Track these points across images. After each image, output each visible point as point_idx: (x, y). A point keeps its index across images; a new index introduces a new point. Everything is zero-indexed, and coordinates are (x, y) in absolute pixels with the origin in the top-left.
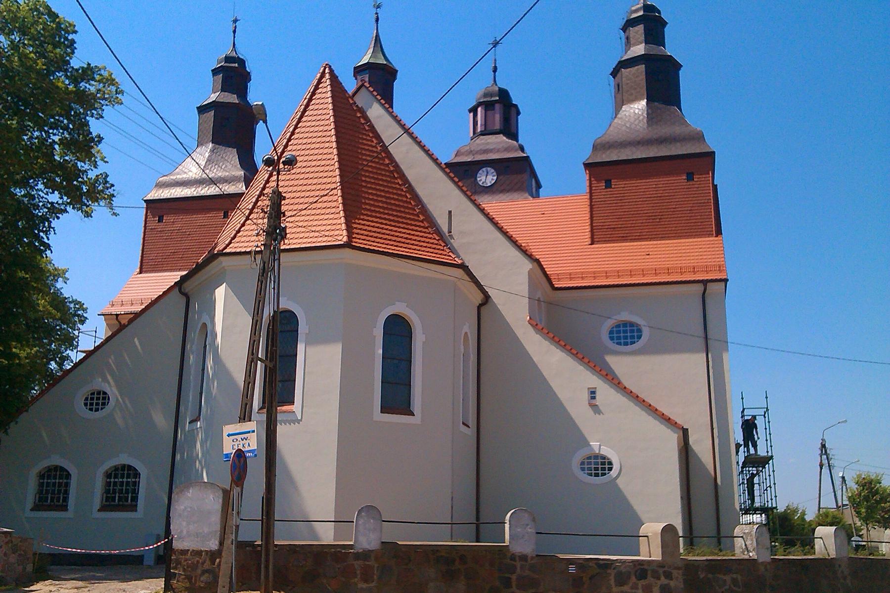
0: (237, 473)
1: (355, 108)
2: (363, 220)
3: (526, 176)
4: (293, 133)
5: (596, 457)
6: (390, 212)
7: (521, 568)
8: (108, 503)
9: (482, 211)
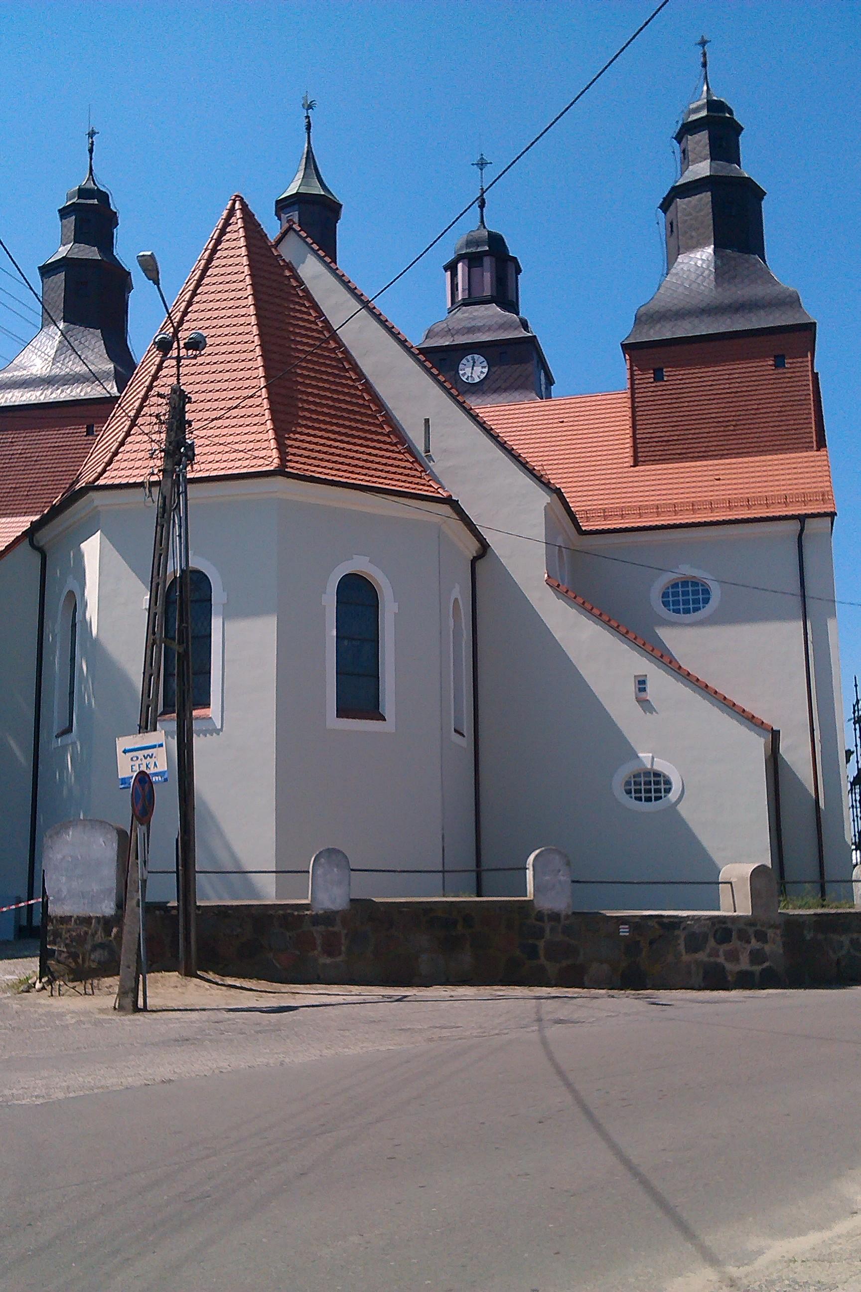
0: (140, 807)
1: (282, 263)
2: (301, 433)
3: (531, 367)
4: (190, 303)
5: (647, 773)
6: (341, 422)
7: (552, 929)
9: (475, 418)
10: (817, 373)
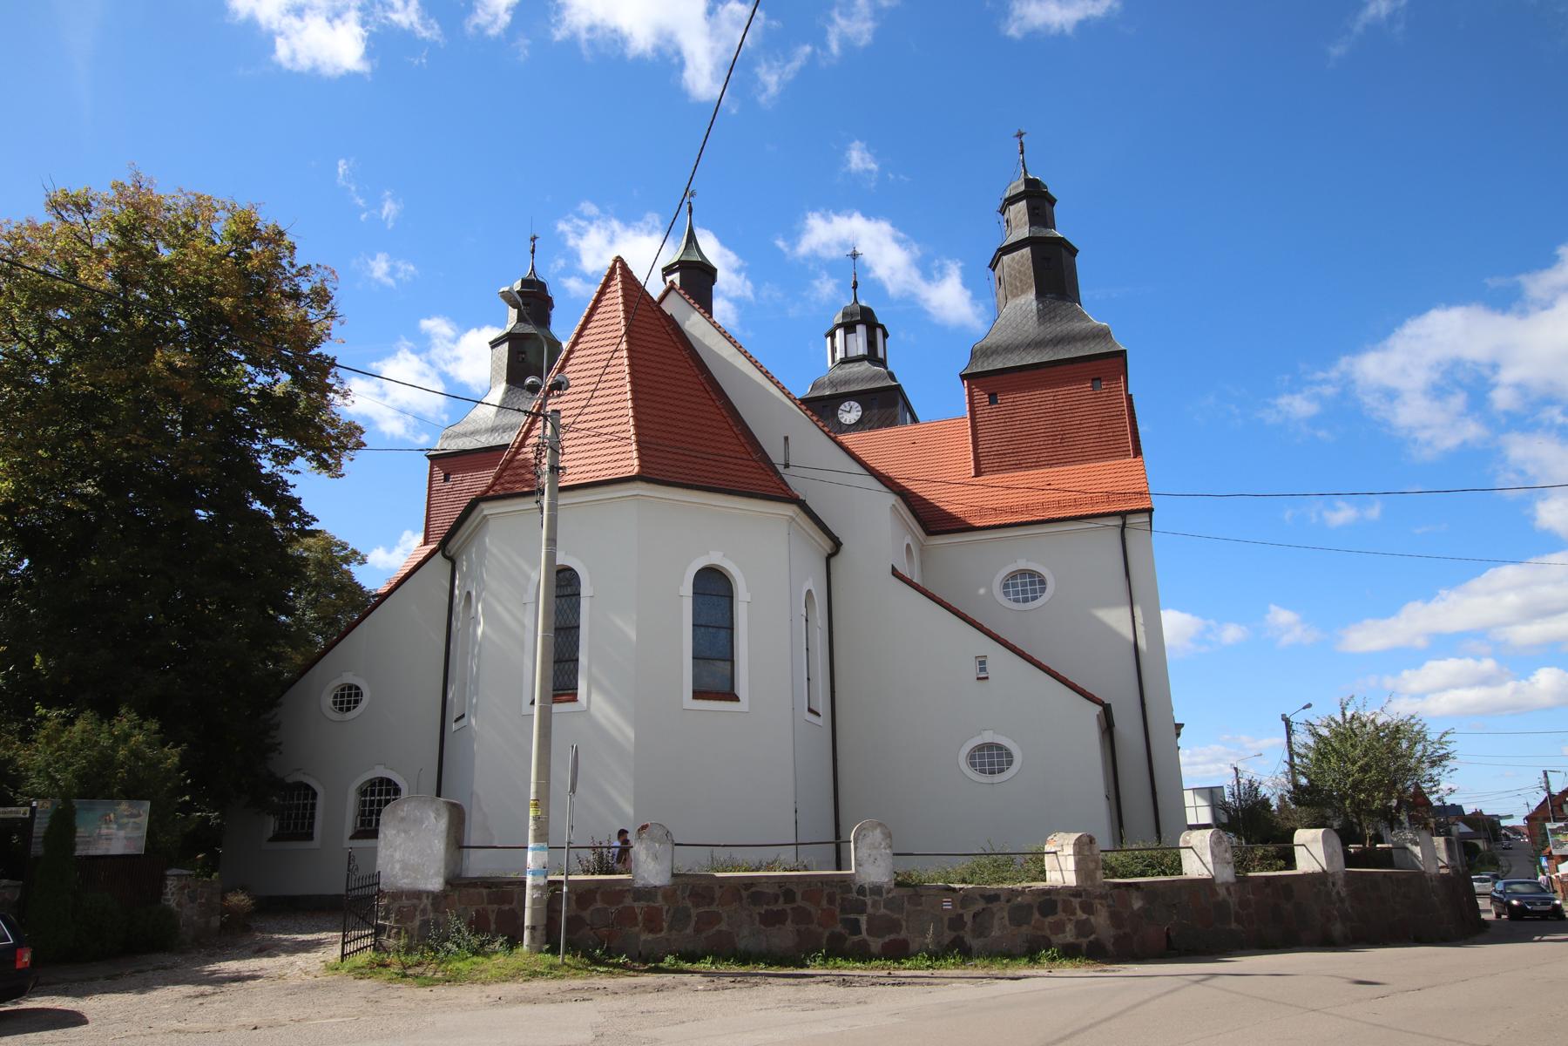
8: (363, 828)
10: (1131, 395)
